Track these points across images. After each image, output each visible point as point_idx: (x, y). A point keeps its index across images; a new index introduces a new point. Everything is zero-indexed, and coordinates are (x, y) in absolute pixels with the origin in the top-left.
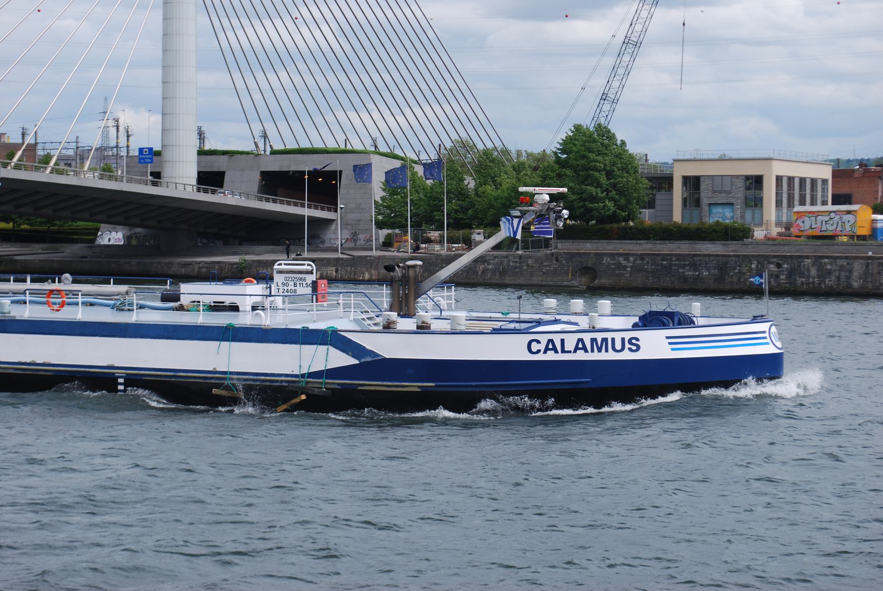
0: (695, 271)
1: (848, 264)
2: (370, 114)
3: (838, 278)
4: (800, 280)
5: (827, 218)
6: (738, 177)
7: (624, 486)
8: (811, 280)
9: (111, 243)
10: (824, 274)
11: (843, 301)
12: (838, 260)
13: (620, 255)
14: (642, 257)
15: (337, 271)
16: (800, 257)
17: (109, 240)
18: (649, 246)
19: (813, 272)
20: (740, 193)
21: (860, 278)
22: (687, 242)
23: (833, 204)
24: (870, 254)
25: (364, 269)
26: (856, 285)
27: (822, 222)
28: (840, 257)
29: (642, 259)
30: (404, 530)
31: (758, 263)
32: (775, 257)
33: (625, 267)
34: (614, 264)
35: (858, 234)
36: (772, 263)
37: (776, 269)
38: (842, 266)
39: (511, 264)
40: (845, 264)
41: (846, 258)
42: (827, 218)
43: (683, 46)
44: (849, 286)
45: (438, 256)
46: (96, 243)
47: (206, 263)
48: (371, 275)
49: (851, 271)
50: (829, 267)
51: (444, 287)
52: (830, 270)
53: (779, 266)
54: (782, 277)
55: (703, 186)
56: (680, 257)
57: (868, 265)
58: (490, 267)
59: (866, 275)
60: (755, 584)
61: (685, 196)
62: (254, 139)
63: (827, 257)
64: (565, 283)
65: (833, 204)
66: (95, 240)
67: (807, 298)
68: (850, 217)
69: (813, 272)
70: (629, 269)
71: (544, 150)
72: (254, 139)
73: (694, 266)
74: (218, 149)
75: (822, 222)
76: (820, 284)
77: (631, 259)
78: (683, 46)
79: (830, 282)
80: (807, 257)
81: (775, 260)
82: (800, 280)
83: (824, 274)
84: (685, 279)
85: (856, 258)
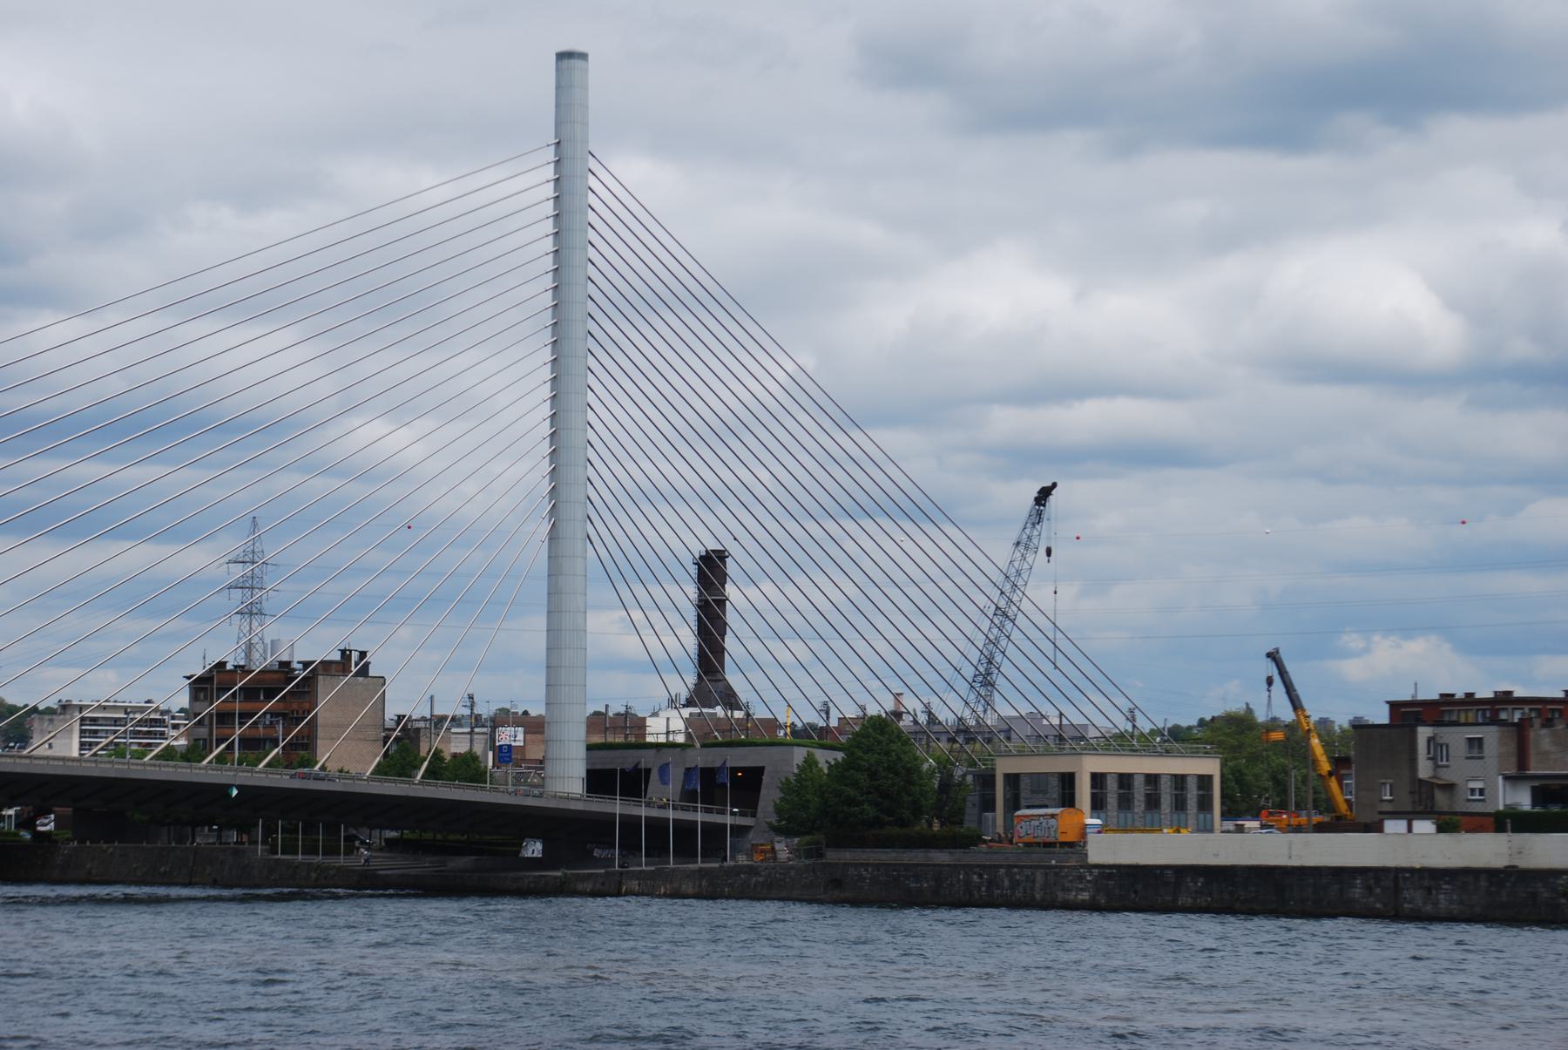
0: (917, 883)
1: (1032, 874)
3: (1025, 889)
5: (1037, 823)
6: (1052, 774)
7: (48, 941)
8: (1005, 892)
9: (535, 855)
10: (1015, 885)
11: (1554, 929)
12: (1025, 870)
13: (862, 864)
14: (878, 866)
15: (639, 885)
16: (995, 866)
17: (533, 853)
18: (894, 855)
19: (1006, 883)
20: (1025, 794)
21: (1041, 890)
22: (922, 850)
23: (282, 853)
24: (1053, 862)
25: (661, 882)
26: (1038, 896)
28: (1026, 867)
29: (878, 870)
30: (283, 1029)
31: (966, 873)
32: (978, 866)
33: (865, 878)
34: (856, 875)
35: (1061, 840)
36: (975, 873)
37: (978, 880)
38: (1027, 876)
39: (778, 875)
40: (1030, 873)
41: (1031, 867)
42: (1037, 823)
43: (1055, 610)
46: (521, 855)
47: (534, 877)
49: (1034, 882)
50: (1018, 877)
52: (1018, 881)
53: (981, 876)
54: (983, 889)
55: (1022, 786)
56: (907, 867)
57: (1046, 874)
58: (761, 879)
61: (1008, 797)
63: (1016, 866)
64: (818, 897)
65: (282, 853)
66: (519, 852)
67: (1378, 920)
68: (1052, 822)
69: (1006, 883)
70: (868, 881)
71: (1247, 704)
76: (1011, 896)
77: (870, 869)
78: (1055, 610)
79: (1019, 894)
80: (1001, 866)
81: (977, 870)
83: (1015, 885)
85: (1037, 867)
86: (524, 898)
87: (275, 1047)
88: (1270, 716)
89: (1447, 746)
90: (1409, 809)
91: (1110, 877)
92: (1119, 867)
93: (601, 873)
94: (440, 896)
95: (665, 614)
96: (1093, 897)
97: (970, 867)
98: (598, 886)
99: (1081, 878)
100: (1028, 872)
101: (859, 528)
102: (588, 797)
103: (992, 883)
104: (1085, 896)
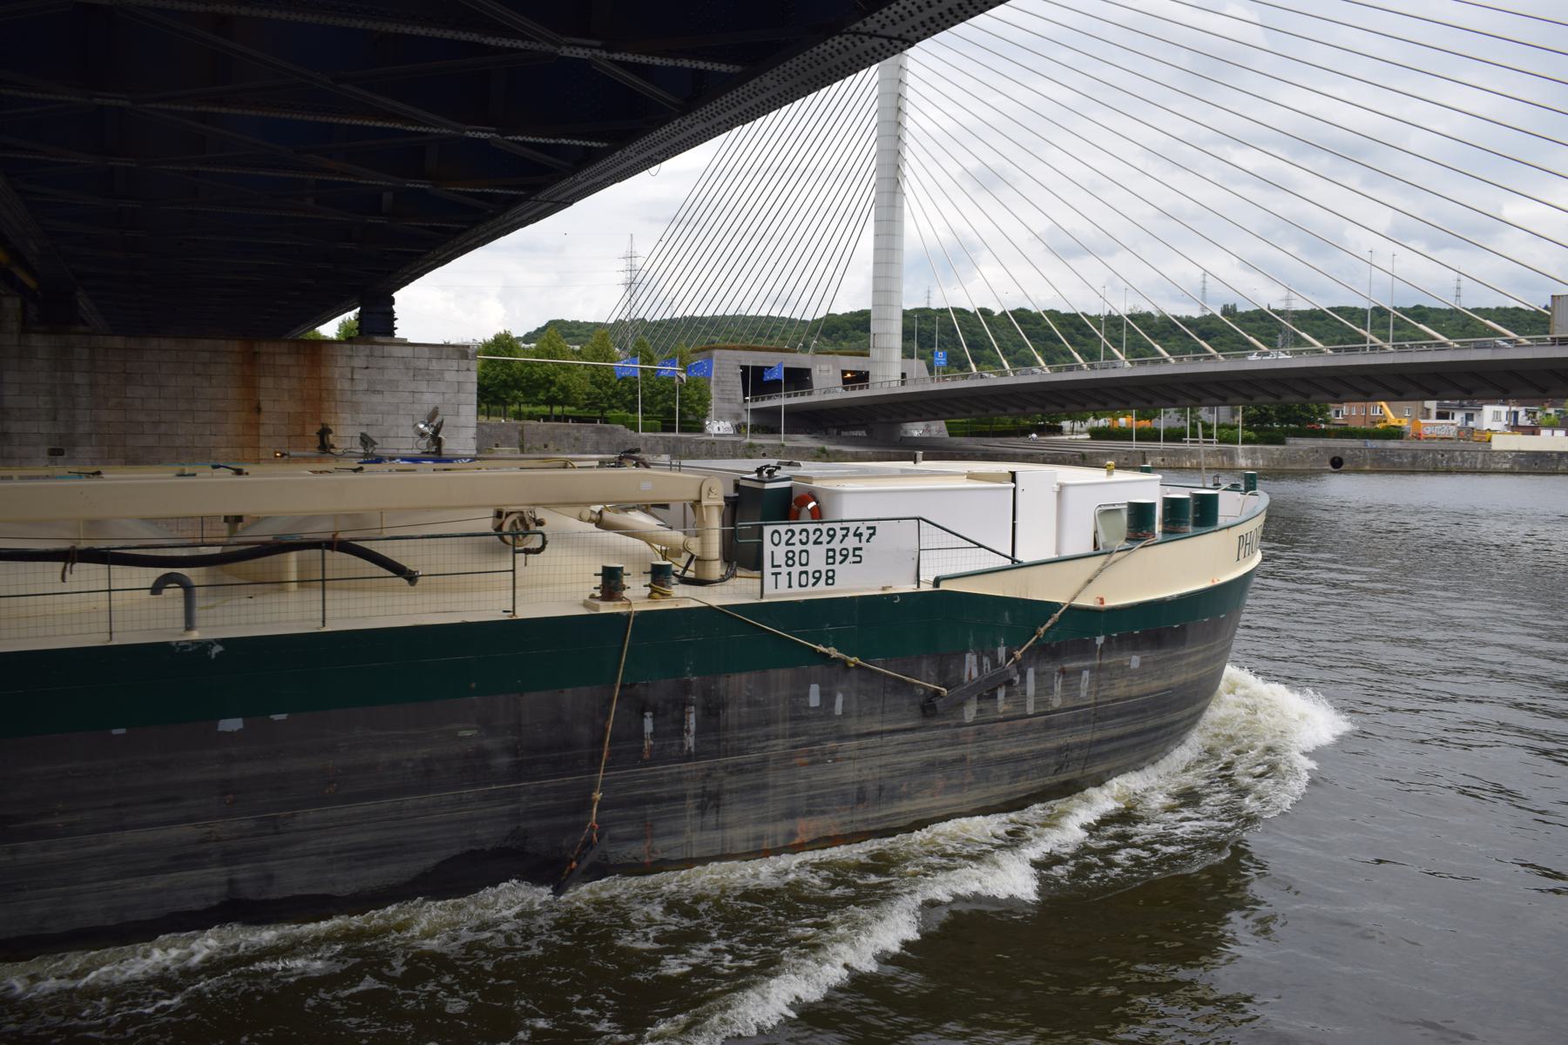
2: (998, 553)
4: (1453, 464)
19: (1460, 459)
26: (1479, 466)
27: (685, 505)
44: (1475, 468)
45: (639, 953)
48: (1192, 463)
51: (1079, 672)
53: (1442, 456)
59: (1484, 461)
60: (1252, 678)
62: (1015, 490)
69: (1460, 459)
72: (1015, 490)
73: (1399, 456)
74: (566, 319)
75: (685, 505)
82: (1453, 464)
84: (1394, 464)
86: (1167, 754)
87: (1188, 1040)
88: (1557, 328)
89: (860, 562)
90: (321, 592)
91: (1522, 456)
92: (1527, 452)
93: (844, 702)
94: (724, 549)
95: (937, 202)
96: (1512, 468)
97: (1436, 451)
98: (1122, 461)
99: (1505, 457)
100: (1473, 453)
101: (1034, 176)
102: (1205, 442)
103: (1452, 459)
104: (1507, 466)
